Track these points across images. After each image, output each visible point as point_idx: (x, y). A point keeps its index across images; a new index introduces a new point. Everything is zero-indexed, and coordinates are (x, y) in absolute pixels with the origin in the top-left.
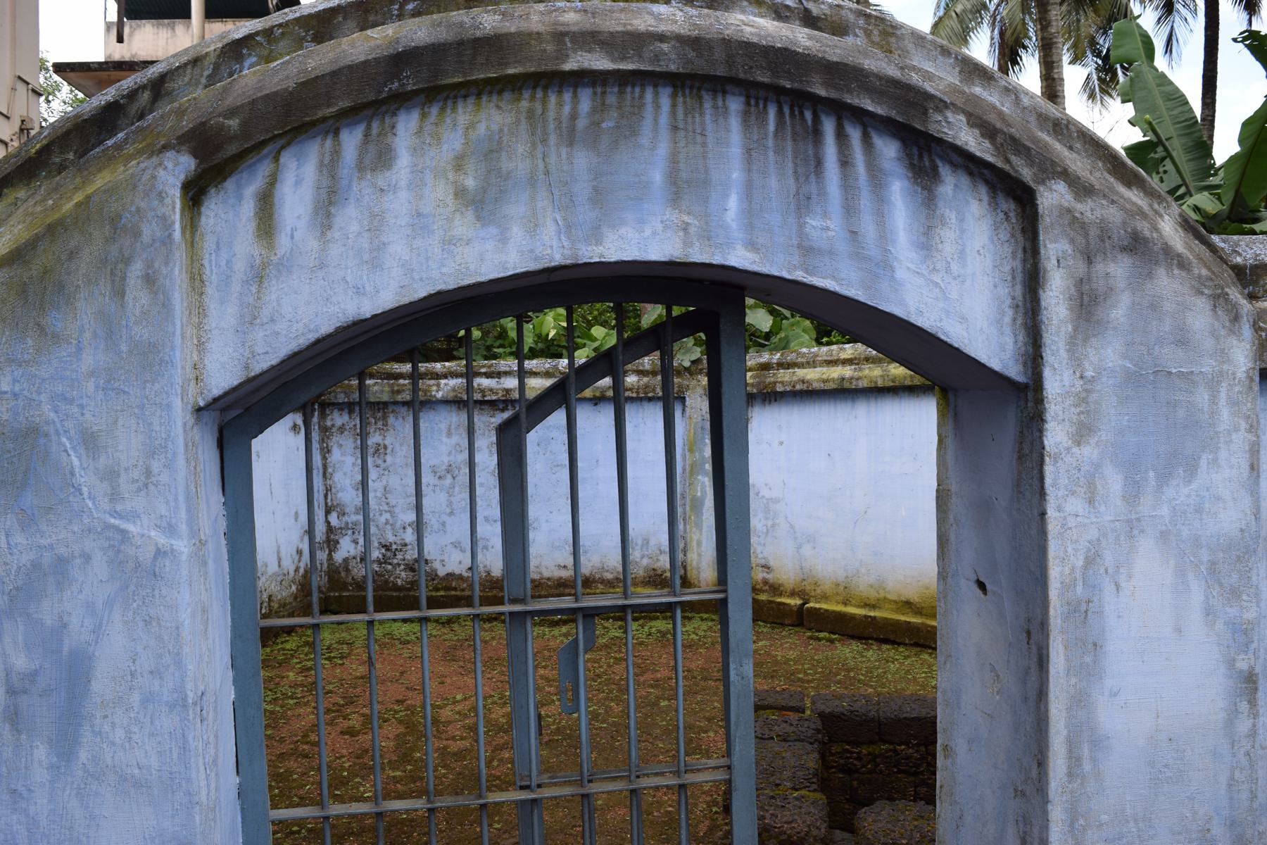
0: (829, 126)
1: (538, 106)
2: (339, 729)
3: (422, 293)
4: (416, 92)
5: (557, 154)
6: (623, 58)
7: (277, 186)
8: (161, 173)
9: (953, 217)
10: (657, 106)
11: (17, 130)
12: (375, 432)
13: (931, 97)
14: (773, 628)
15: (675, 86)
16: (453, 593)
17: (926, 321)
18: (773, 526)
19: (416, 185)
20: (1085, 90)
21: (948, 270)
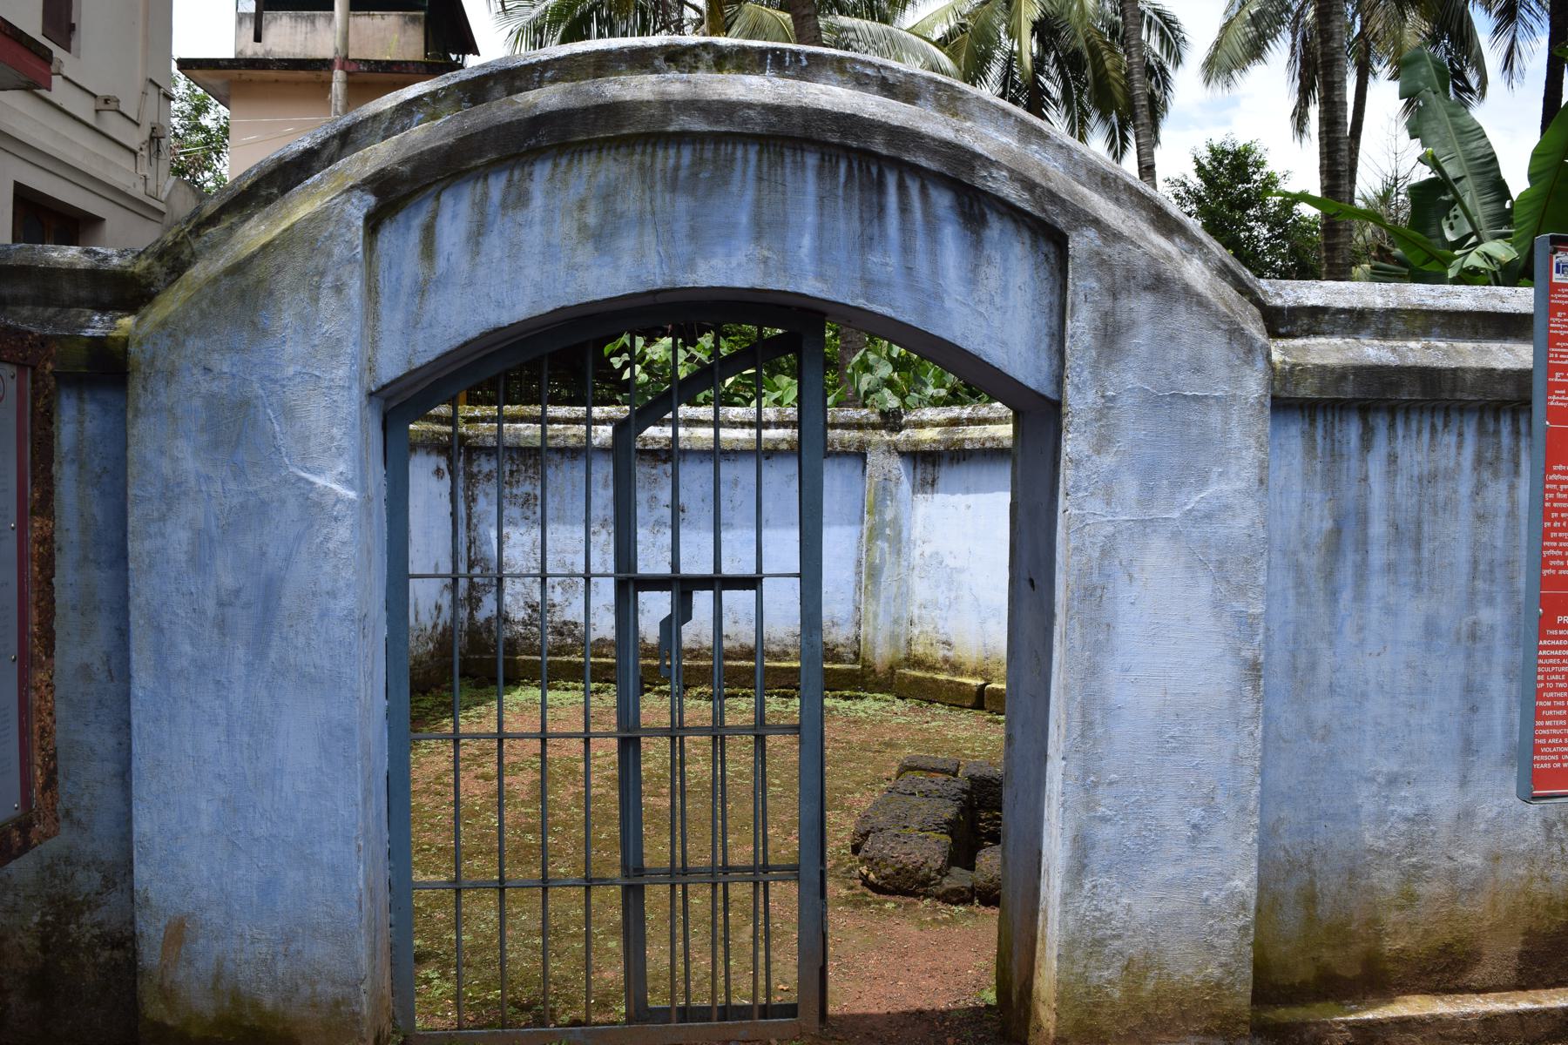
0: (891, 181)
1: (648, 161)
2: (472, 774)
3: (550, 308)
4: (550, 148)
5: (662, 199)
6: (717, 122)
7: (438, 219)
8: (348, 207)
9: (998, 257)
10: (746, 160)
11: (147, 137)
12: (525, 480)
13: (977, 156)
14: (951, 711)
15: (761, 145)
16: (604, 660)
17: (971, 345)
18: (956, 598)
19: (548, 221)
20: (1405, 112)
21: (992, 302)
